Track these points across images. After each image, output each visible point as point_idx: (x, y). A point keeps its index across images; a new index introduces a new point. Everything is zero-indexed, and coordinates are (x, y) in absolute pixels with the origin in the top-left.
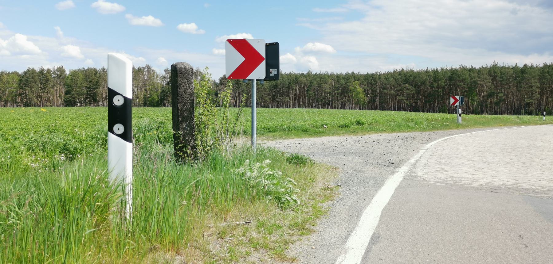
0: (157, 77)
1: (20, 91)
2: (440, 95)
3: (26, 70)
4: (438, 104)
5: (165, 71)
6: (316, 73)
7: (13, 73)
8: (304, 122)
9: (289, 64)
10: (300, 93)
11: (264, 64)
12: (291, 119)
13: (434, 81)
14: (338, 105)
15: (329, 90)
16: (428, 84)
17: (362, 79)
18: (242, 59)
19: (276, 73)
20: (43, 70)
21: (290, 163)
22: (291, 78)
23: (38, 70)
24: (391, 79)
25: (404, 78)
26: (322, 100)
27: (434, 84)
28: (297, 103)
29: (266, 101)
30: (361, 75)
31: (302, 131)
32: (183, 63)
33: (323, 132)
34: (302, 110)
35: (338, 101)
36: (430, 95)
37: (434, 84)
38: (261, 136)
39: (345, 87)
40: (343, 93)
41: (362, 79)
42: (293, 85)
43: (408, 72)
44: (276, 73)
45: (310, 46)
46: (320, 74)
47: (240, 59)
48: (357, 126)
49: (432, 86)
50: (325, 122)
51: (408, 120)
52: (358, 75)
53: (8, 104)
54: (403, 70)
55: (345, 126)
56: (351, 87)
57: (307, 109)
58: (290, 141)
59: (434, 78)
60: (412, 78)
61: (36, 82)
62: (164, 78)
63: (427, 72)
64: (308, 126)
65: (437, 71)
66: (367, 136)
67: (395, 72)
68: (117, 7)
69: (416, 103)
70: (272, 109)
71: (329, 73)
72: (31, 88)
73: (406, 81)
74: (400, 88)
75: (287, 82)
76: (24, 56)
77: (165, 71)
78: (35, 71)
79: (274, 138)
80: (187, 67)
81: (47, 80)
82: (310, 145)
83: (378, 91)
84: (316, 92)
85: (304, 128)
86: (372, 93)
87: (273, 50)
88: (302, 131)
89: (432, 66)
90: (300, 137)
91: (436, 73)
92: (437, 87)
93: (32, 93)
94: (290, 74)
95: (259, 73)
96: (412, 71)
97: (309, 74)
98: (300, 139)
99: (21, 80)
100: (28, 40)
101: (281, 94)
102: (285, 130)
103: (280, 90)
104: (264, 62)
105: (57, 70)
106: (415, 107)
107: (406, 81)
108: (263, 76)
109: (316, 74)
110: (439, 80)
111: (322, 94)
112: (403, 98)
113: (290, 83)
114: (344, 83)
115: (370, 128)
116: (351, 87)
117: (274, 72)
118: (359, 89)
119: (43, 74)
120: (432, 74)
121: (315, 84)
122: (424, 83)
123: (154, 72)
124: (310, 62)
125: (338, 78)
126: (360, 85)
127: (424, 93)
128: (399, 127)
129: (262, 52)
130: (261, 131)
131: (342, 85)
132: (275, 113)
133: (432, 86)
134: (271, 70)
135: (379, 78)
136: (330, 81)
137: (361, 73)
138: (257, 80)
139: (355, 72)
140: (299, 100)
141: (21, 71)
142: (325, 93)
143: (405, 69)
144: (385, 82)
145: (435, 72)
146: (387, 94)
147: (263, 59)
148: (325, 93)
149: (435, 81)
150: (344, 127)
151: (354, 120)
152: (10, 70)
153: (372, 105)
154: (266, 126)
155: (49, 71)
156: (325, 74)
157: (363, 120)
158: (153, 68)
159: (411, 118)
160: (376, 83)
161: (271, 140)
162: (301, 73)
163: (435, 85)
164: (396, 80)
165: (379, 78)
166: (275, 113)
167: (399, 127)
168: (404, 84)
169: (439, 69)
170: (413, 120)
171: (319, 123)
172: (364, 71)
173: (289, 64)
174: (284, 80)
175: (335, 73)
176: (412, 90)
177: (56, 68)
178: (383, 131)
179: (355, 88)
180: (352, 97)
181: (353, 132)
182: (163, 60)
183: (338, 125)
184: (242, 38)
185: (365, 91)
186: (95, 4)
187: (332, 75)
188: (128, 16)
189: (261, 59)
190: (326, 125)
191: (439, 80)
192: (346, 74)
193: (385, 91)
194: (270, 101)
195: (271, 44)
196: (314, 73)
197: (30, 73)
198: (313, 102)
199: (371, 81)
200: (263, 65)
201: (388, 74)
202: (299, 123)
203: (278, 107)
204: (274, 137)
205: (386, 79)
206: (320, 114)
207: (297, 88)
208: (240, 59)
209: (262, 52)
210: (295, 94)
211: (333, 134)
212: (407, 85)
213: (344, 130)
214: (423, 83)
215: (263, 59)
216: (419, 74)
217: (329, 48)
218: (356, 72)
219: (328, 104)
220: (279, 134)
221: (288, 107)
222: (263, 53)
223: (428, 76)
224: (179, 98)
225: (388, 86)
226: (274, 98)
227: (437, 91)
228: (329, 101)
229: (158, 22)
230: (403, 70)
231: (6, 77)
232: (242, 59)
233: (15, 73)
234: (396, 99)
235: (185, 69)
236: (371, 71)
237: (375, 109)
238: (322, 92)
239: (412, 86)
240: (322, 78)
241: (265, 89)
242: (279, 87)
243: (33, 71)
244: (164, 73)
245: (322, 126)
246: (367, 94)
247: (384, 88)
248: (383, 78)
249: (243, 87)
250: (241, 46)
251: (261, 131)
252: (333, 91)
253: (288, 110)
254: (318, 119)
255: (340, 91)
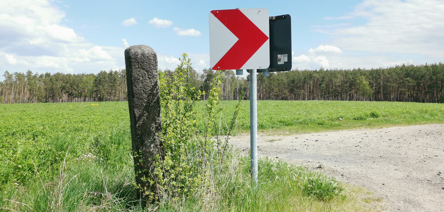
0: (198, 76)
1: (95, 89)
2: (439, 87)
3: (99, 72)
4: (437, 94)
5: (203, 71)
6: (327, 70)
7: (90, 75)
8: (320, 114)
9: (305, 58)
10: (313, 86)
11: (266, 46)
12: (306, 112)
13: (433, 75)
14: (347, 98)
15: (338, 84)
16: (427, 77)
17: (367, 74)
18: (234, 39)
19: (286, 60)
20: (112, 72)
21: (309, 195)
22: (305, 74)
23: (108, 72)
24: (394, 74)
25: (405, 72)
26: (333, 93)
27: (433, 77)
28: (312, 96)
29: (285, 94)
30: (366, 71)
31: (318, 124)
32: (140, 47)
33: (340, 125)
34: (316, 102)
35: (347, 93)
36: (430, 87)
37: (433, 77)
38: (278, 130)
39: (352, 81)
40: (350, 86)
41: (367, 74)
42: (307, 80)
43: (409, 67)
44: (286, 60)
45: (321, 48)
46: (331, 71)
47: (230, 39)
48: (372, 119)
49: (431, 79)
50: (340, 114)
51: (421, 112)
52: (363, 71)
53: (87, 99)
54: (404, 65)
55: (360, 119)
56: (358, 81)
57: (321, 101)
58: (307, 136)
59: (433, 72)
60: (413, 73)
61: (106, 81)
62: (202, 76)
63: (426, 67)
64: (324, 119)
65: (435, 65)
66: (385, 129)
67: (397, 67)
68: (167, 22)
69: (417, 94)
70: (290, 102)
71: (339, 69)
72: (103, 86)
73: (407, 75)
74: (401, 81)
75: (303, 78)
76: (100, 62)
77: (203, 71)
78: (106, 73)
79: (291, 133)
80: (146, 52)
81: (115, 80)
82: (328, 142)
83: (382, 84)
84: (328, 85)
85: (320, 121)
86: (376, 86)
87: (281, 27)
88: (318, 124)
89: (430, 62)
90: (317, 131)
91: (435, 67)
92: (436, 80)
93: (105, 89)
94: (305, 71)
95: (261, 58)
96: (412, 66)
97: (321, 71)
98: (316, 134)
99: (96, 80)
100: (103, 50)
101: (298, 88)
102: (301, 123)
103: (297, 84)
104: (267, 43)
105: (122, 72)
106: (416, 97)
107: (407, 75)
108: (266, 64)
109: (327, 71)
110: (439, 73)
111: (332, 87)
112: (405, 90)
113: (305, 78)
114: (351, 77)
115: (386, 120)
116: (358, 81)
117: (282, 59)
118: (365, 82)
119: (111, 75)
120: (431, 69)
121: (327, 79)
122: (423, 77)
123: (195, 72)
124: (321, 61)
125: (346, 73)
126: (366, 79)
127: (424, 85)
128: (414, 118)
129: (265, 28)
130: (277, 124)
131: (349, 79)
132: (292, 105)
133: (431, 79)
134: (279, 56)
135: (383, 73)
136: (339, 76)
137: (366, 69)
138: (258, 71)
139: (361, 69)
140: (313, 92)
141: (96, 73)
142: (335, 86)
143: (406, 65)
144: (388, 76)
145: (434, 67)
146: (390, 86)
147: (266, 38)
148: (335, 86)
149: (434, 75)
150: (359, 120)
151: (369, 112)
152: (88, 72)
153: (376, 97)
154: (282, 120)
155: (116, 72)
156: (335, 71)
157: (378, 112)
158: (194, 69)
159: (424, 110)
160: (380, 78)
161: (287, 135)
162: (315, 70)
163: (434, 78)
164: (398, 74)
165: (383, 73)
166: (292, 105)
167: (414, 118)
168: (405, 77)
169: (438, 64)
170: (426, 112)
171: (334, 116)
172: (368, 67)
173: (305, 58)
174: (300, 76)
175: (343, 69)
176: (412, 82)
177: (121, 70)
178: (399, 123)
179: (362, 82)
180: (358, 89)
181: (369, 124)
182: (202, 62)
183: (354, 117)
184: (234, 8)
185: (370, 84)
186: (151, 22)
187: (341, 71)
188: (176, 29)
189: (261, 38)
190: (341, 117)
191: (439, 73)
192: (354, 70)
193: (388, 84)
194: (288, 94)
195: (279, 18)
196: (325, 70)
197: (103, 74)
198: (325, 94)
199: (375, 75)
200: (265, 48)
201: (391, 69)
202: (315, 116)
203: (295, 100)
204: (290, 130)
205: (389, 73)
206: (333, 106)
207: (312, 82)
208: (230, 39)
209: (265, 28)
210: (310, 88)
211: (349, 127)
212: (408, 78)
213: (360, 123)
214: (423, 76)
215: (266, 38)
216: (418, 69)
217: (336, 50)
218: (362, 68)
219: (337, 96)
220: (295, 127)
221: (304, 99)
222: (265, 30)
223: (428, 70)
224: (135, 99)
225: (391, 80)
226: (291, 91)
227: (436, 83)
228: (339, 93)
229: (198, 33)
230: (404, 65)
231: (85, 78)
232: (234, 39)
233: (92, 75)
234: (398, 91)
235: (143, 54)
236: (376, 67)
237: (380, 100)
238: (333, 86)
239: (413, 79)
240: (333, 74)
241: (284, 84)
242: (296, 82)
243: (105, 73)
244: (203, 72)
245: (338, 119)
246: (372, 86)
247: (388, 81)
248: (386, 72)
249: (266, 82)
250: (232, 19)
251: (277, 124)
252: (342, 85)
253: (303, 102)
254: (332, 112)
255: (348, 84)
